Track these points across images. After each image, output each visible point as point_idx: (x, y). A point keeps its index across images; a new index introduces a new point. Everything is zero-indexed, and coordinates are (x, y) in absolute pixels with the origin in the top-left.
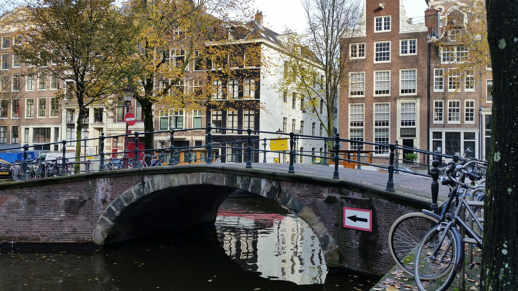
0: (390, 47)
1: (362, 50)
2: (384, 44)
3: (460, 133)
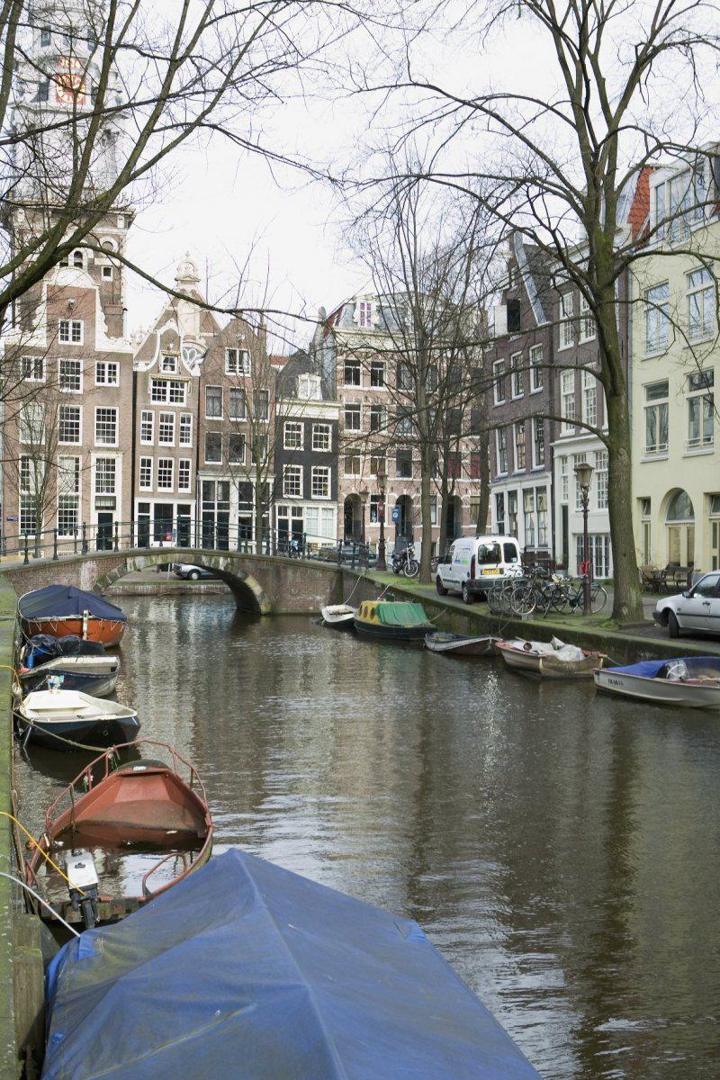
0: (117, 416)
1: (322, 430)
2: (109, 411)
3: (172, 505)
